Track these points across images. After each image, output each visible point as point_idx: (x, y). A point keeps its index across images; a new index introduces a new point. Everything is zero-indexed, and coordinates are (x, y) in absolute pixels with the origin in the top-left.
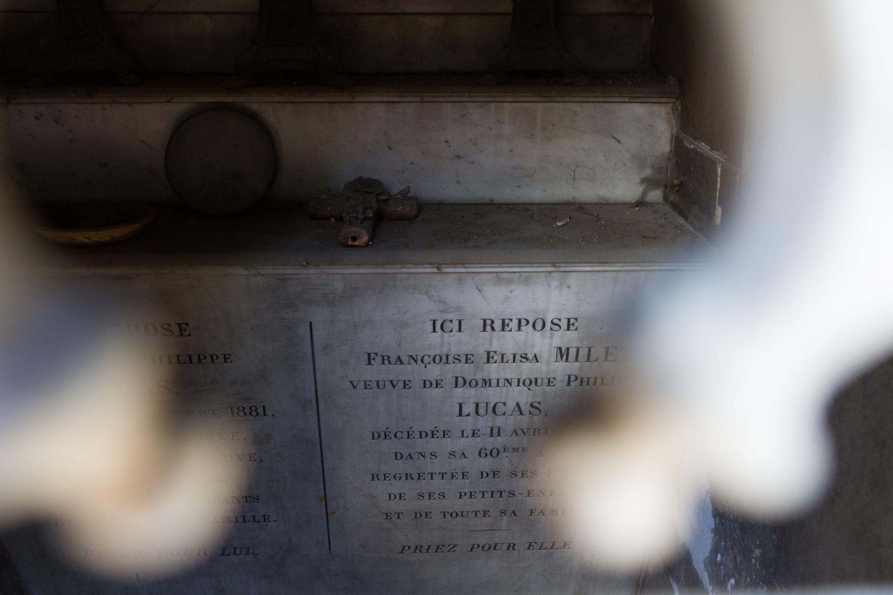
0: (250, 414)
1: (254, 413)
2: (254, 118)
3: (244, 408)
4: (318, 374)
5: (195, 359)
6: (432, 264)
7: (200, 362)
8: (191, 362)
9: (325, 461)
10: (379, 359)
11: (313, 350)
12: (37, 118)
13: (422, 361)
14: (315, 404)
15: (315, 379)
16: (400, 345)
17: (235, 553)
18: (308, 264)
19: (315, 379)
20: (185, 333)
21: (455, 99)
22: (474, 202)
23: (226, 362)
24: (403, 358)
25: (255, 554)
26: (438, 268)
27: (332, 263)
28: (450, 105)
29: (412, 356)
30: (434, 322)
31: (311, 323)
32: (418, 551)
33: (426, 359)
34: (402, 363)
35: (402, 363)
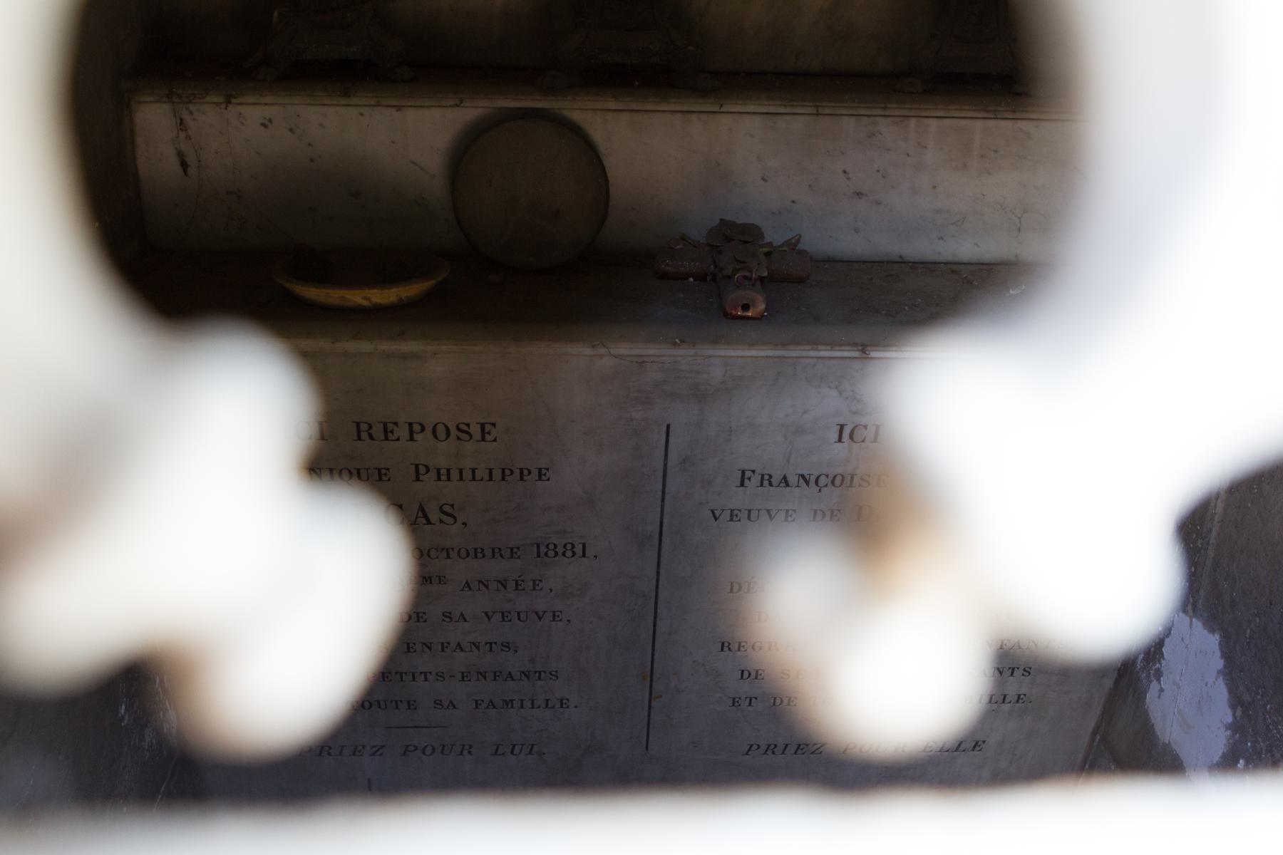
0: (564, 554)
1: (569, 553)
2: (576, 132)
3: (556, 546)
4: (667, 497)
5: (497, 475)
6: (855, 345)
7: (503, 479)
8: (491, 479)
9: (658, 622)
10: (756, 480)
11: (665, 465)
12: (264, 125)
13: (816, 482)
14: (657, 541)
15: (662, 506)
16: (788, 461)
17: (512, 752)
18: (682, 341)
19: (662, 506)
20: (488, 437)
21: (862, 112)
22: (877, 259)
23: (540, 479)
24: (790, 479)
25: (541, 754)
26: (863, 351)
27: (716, 341)
28: (852, 119)
29: (803, 476)
30: (842, 427)
31: (668, 426)
32: (769, 752)
33: (823, 480)
34: (787, 485)
35: (787, 485)
